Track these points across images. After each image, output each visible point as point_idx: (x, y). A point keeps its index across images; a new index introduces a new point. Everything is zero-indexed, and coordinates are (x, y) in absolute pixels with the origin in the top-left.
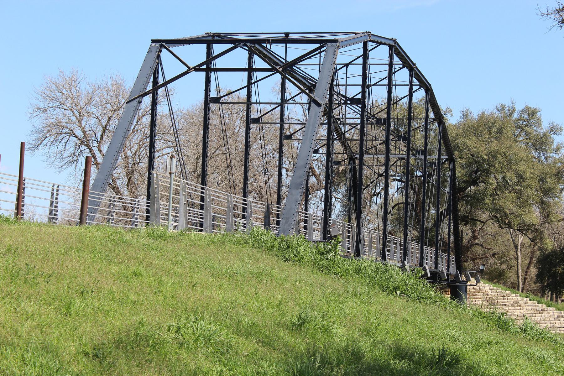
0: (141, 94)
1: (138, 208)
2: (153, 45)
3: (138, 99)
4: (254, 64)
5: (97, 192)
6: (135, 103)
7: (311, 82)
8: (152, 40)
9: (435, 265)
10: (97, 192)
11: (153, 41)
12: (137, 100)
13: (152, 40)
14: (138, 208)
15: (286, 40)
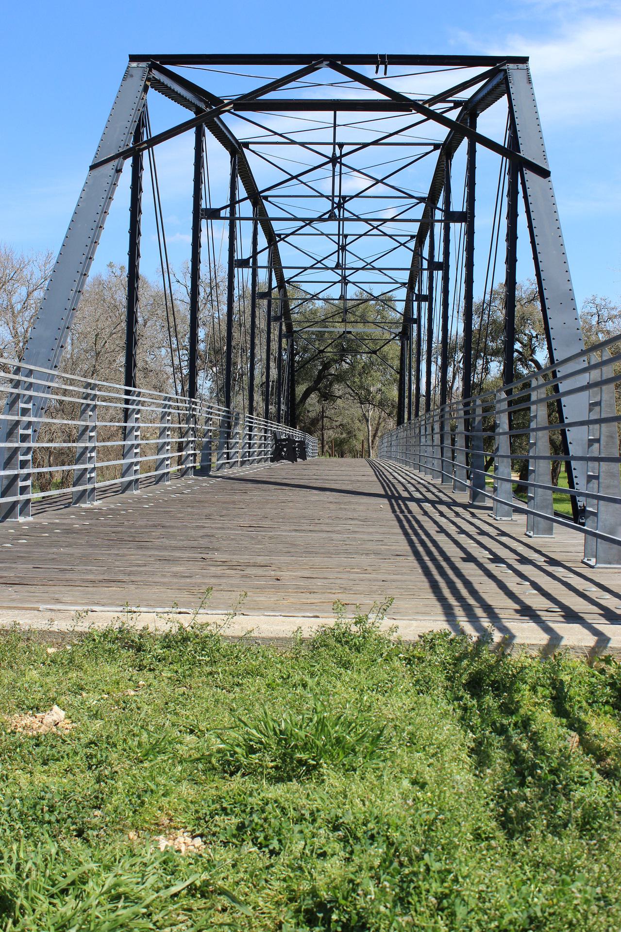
0: (121, 151)
1: (138, 412)
2: (134, 64)
3: (117, 161)
4: (204, 153)
5: (76, 389)
6: (109, 168)
7: (395, 492)
8: (130, 55)
9: (420, 563)
10: (76, 389)
11: (133, 58)
12: (115, 163)
13: (130, 55)
14: (138, 412)
15: (325, 214)
